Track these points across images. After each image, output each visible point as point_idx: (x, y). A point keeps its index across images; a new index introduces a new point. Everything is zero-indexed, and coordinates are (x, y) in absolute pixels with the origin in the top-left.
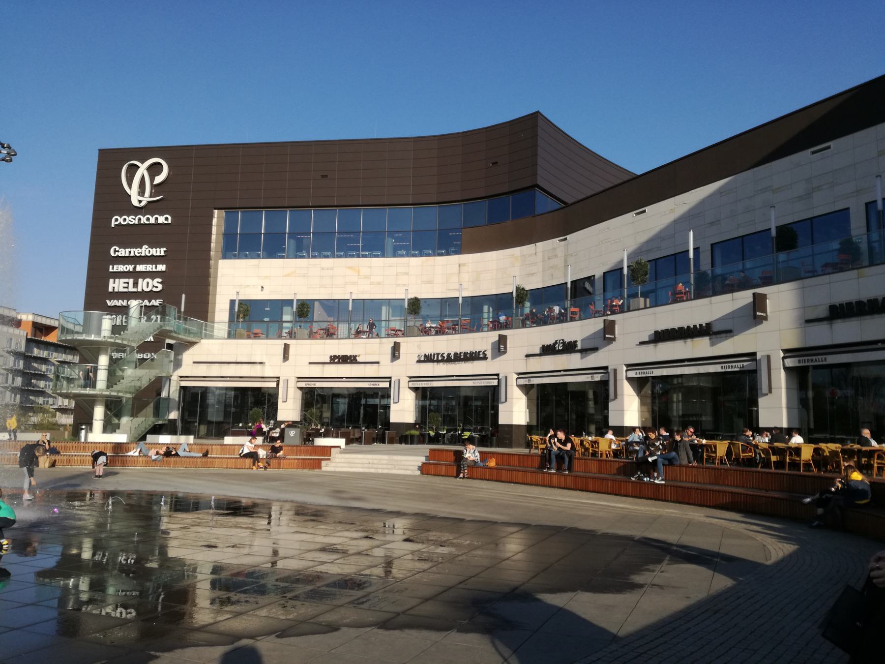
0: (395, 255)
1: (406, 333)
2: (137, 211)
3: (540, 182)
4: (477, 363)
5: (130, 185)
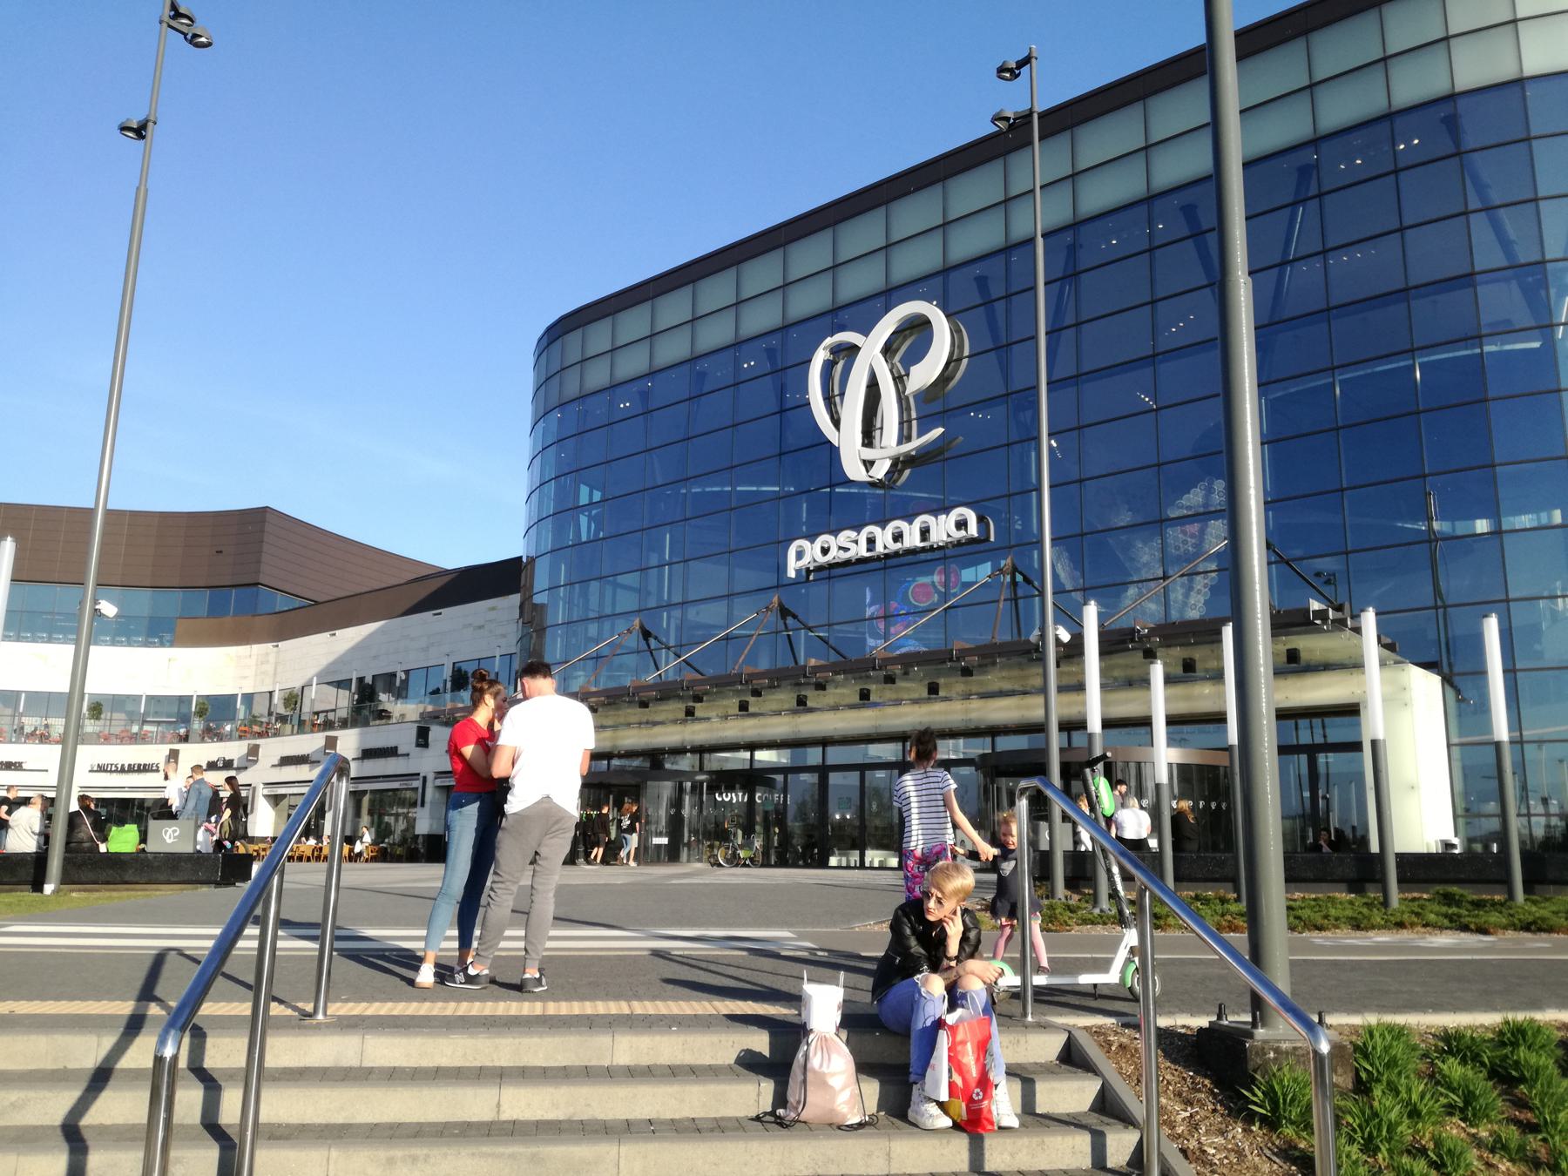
2: (883, 501)
4: (149, 775)
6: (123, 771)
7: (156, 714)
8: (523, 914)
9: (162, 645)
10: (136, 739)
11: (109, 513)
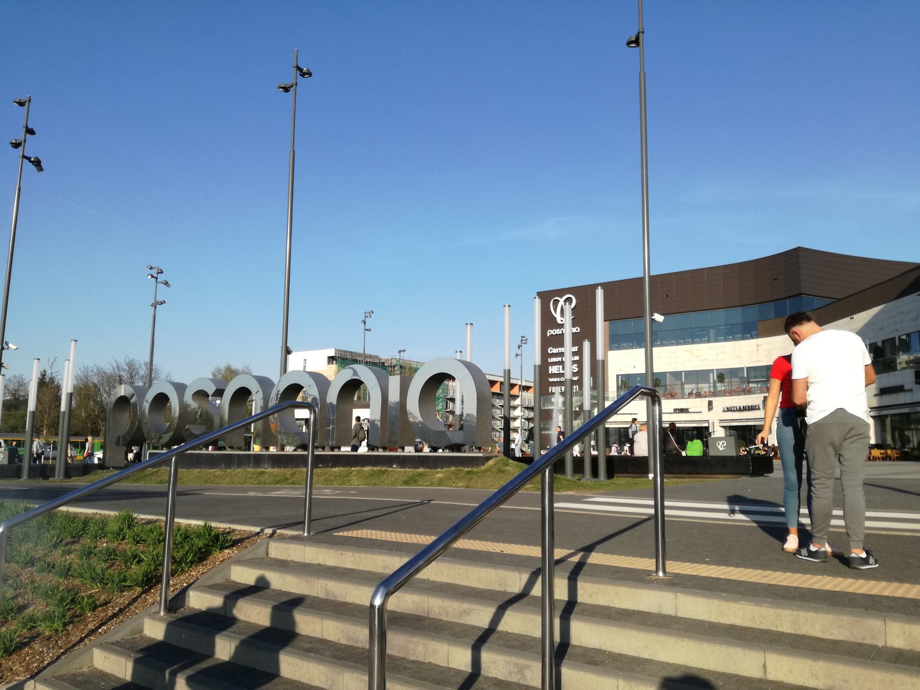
0: (716, 341)
1: (715, 394)
3: (803, 291)
4: (755, 412)
5: (555, 311)
6: (740, 410)
7: (755, 377)
8: (840, 502)
9: (752, 338)
10: (748, 392)
11: (651, 277)
